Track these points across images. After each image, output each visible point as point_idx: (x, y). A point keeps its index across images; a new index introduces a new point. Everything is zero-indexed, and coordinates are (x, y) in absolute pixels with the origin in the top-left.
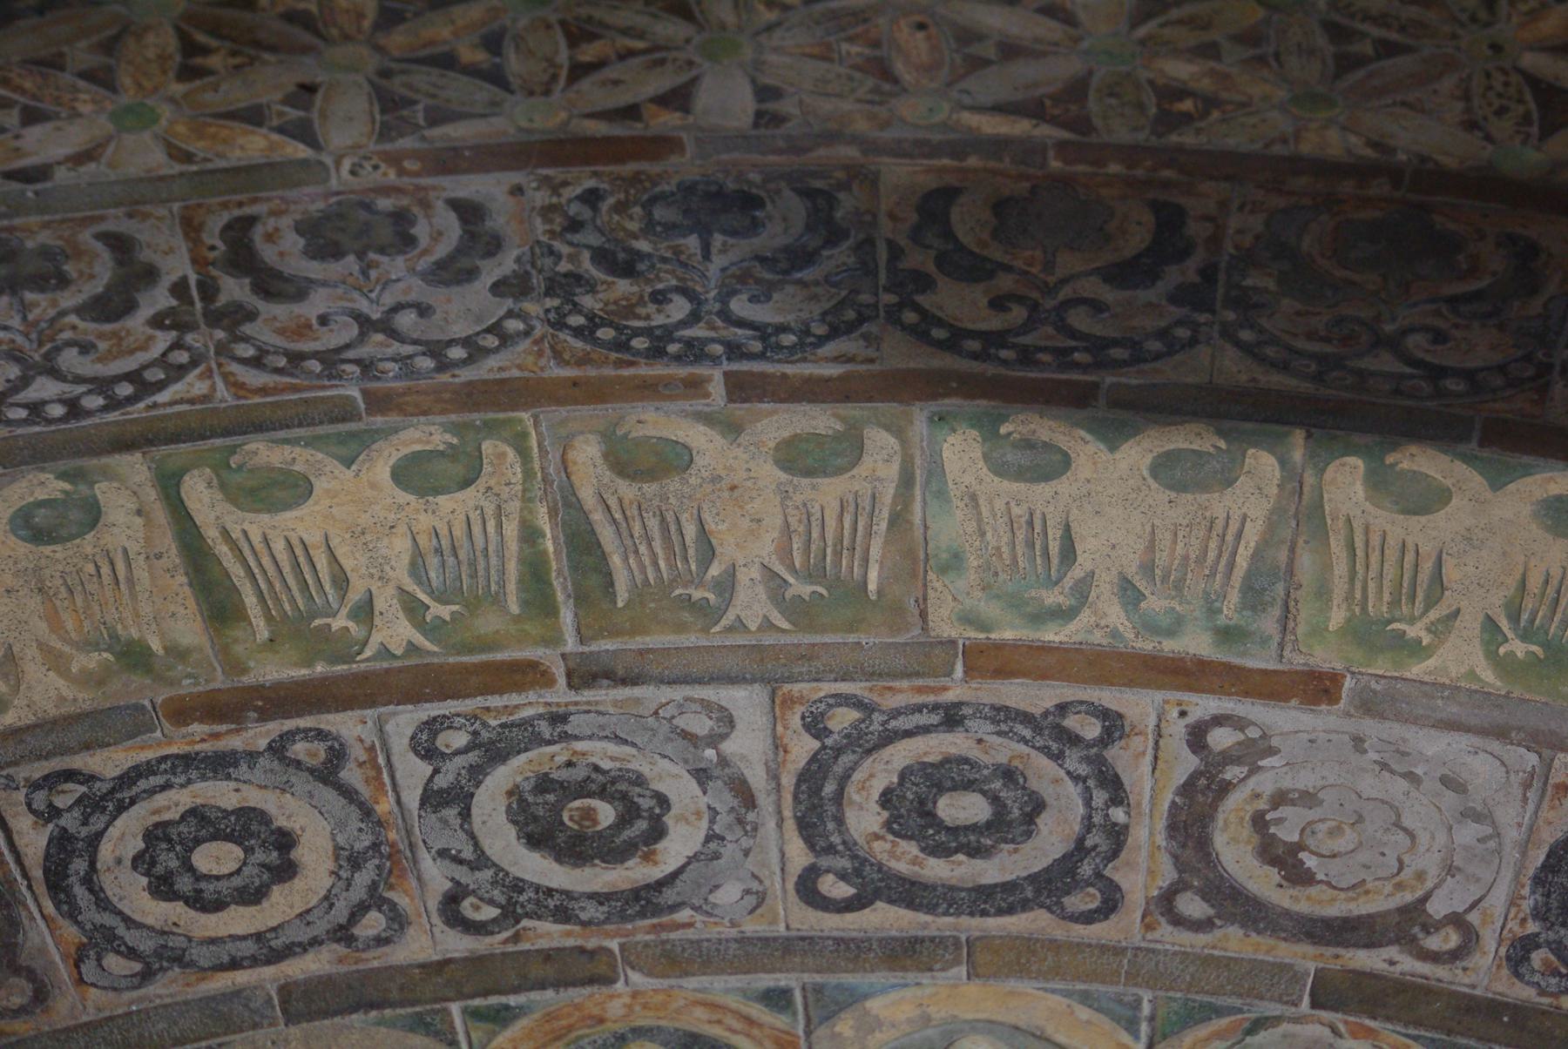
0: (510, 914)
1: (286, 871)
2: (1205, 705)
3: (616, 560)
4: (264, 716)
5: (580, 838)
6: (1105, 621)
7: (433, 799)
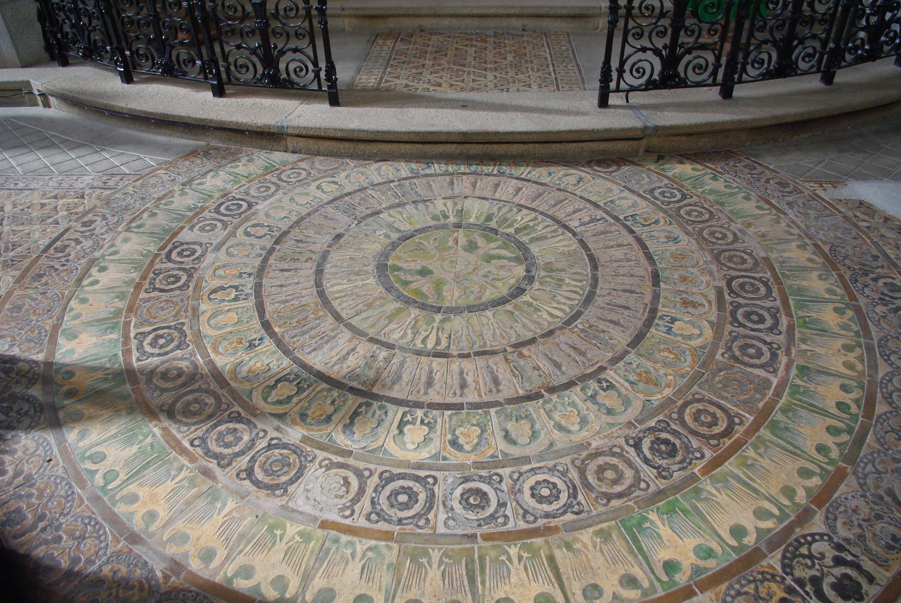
0: (490, 477)
1: (532, 488)
2: (348, 522)
3: (464, 573)
4: (539, 528)
5: (477, 494)
6: (361, 545)
7: (504, 505)
